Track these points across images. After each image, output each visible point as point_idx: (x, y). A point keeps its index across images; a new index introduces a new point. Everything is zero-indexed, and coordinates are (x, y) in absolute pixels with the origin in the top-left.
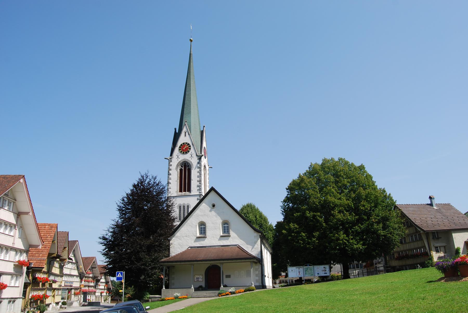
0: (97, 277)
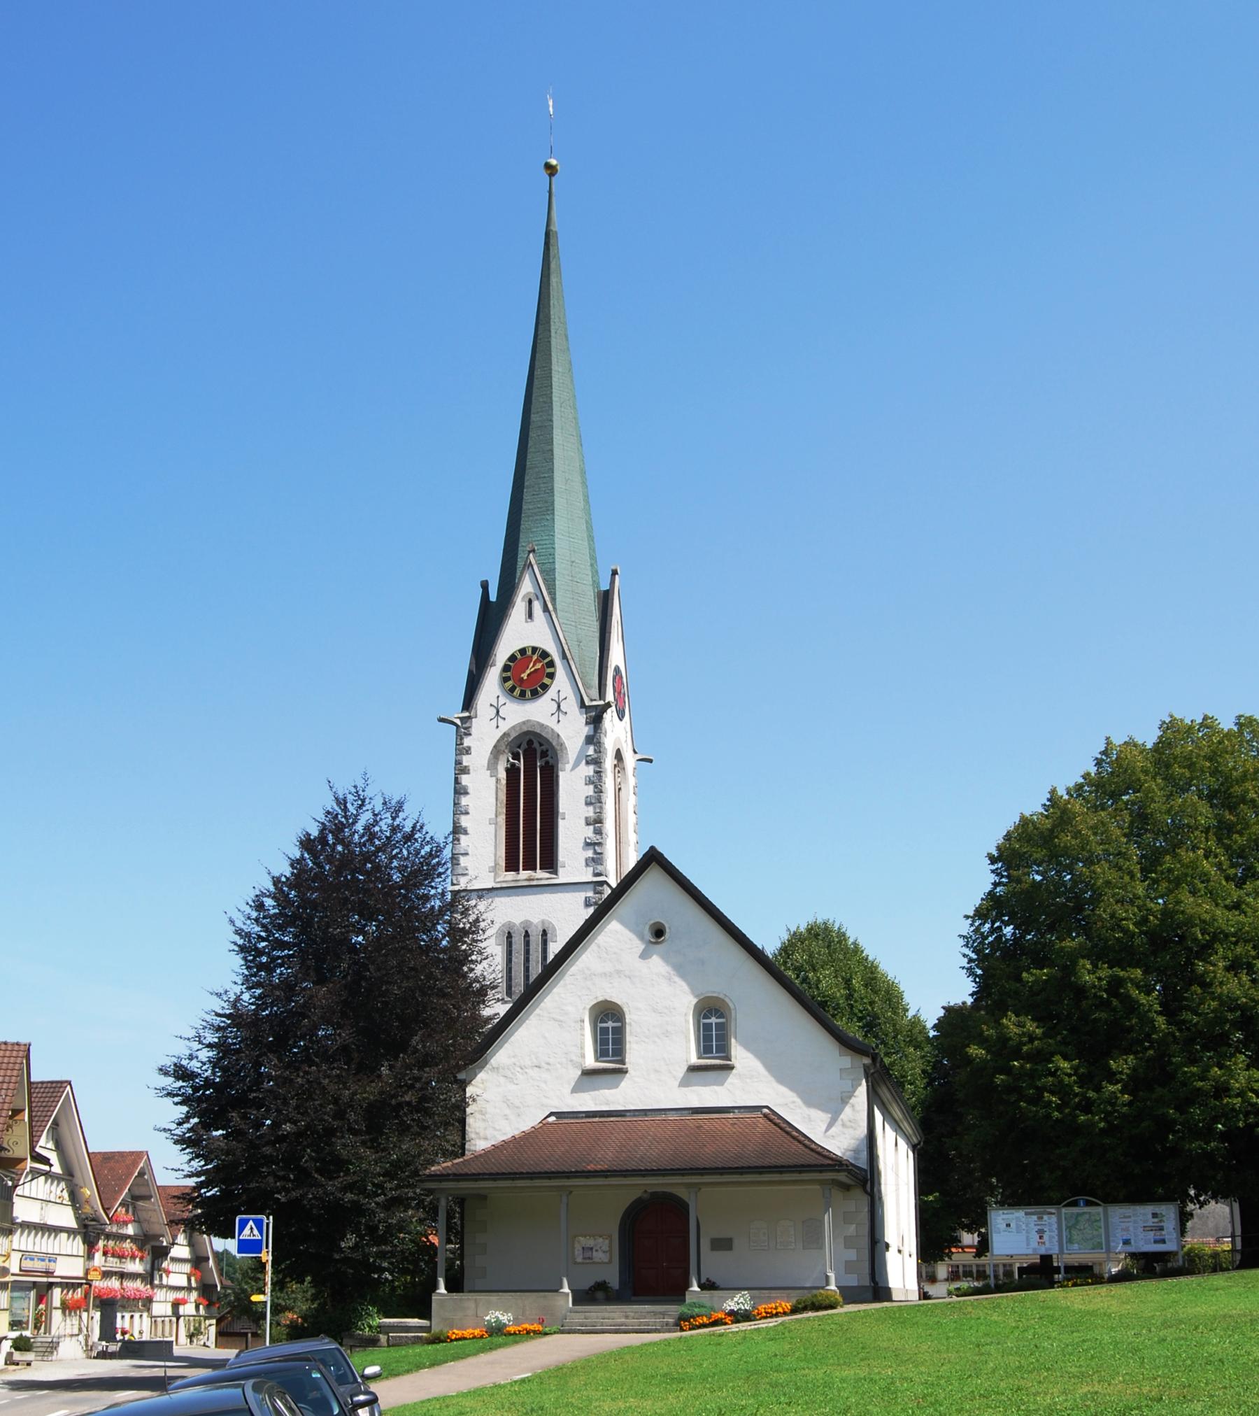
0: (157, 1237)
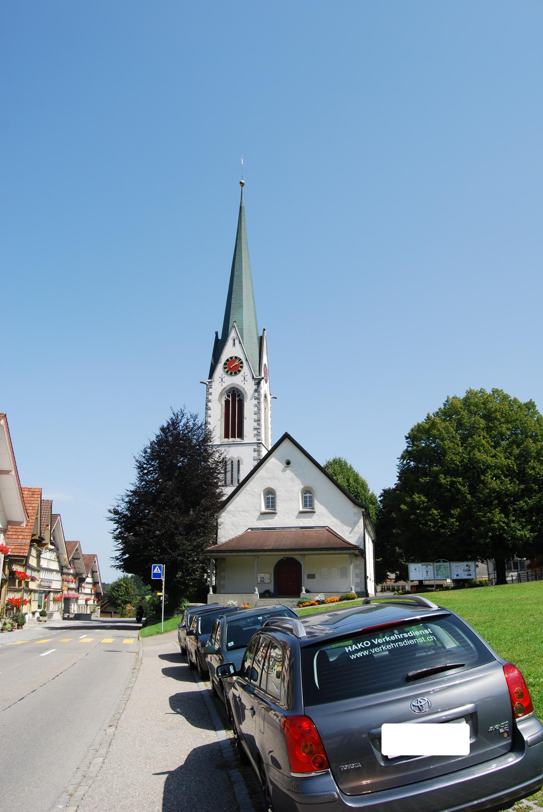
0: (81, 574)
